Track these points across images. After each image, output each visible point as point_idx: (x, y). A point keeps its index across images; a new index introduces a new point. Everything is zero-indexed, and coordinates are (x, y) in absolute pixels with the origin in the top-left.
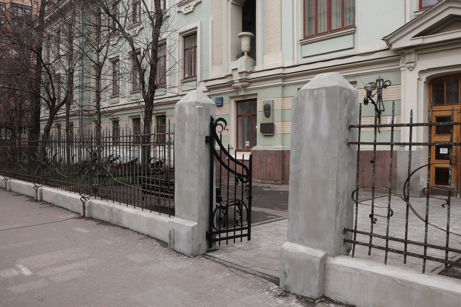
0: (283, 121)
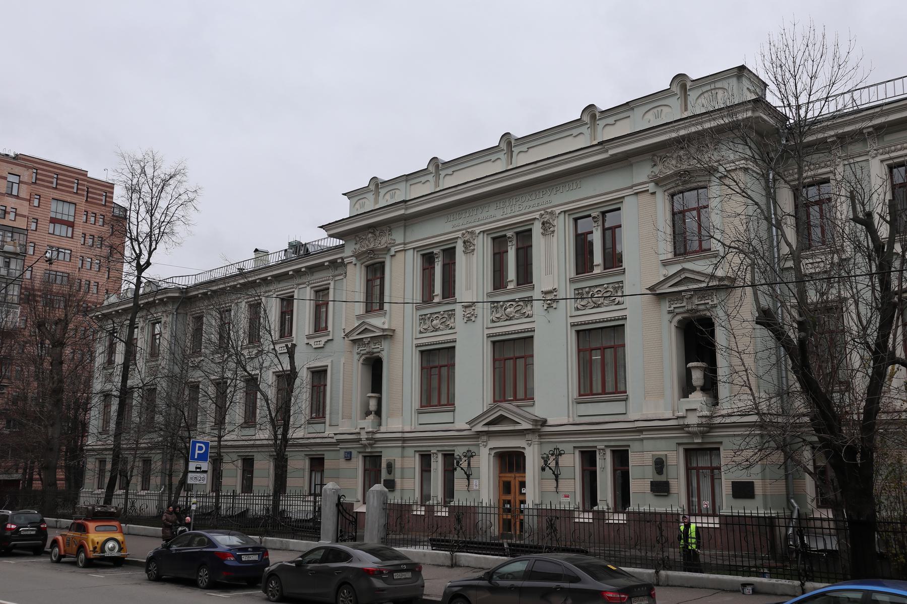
0: (402, 478)
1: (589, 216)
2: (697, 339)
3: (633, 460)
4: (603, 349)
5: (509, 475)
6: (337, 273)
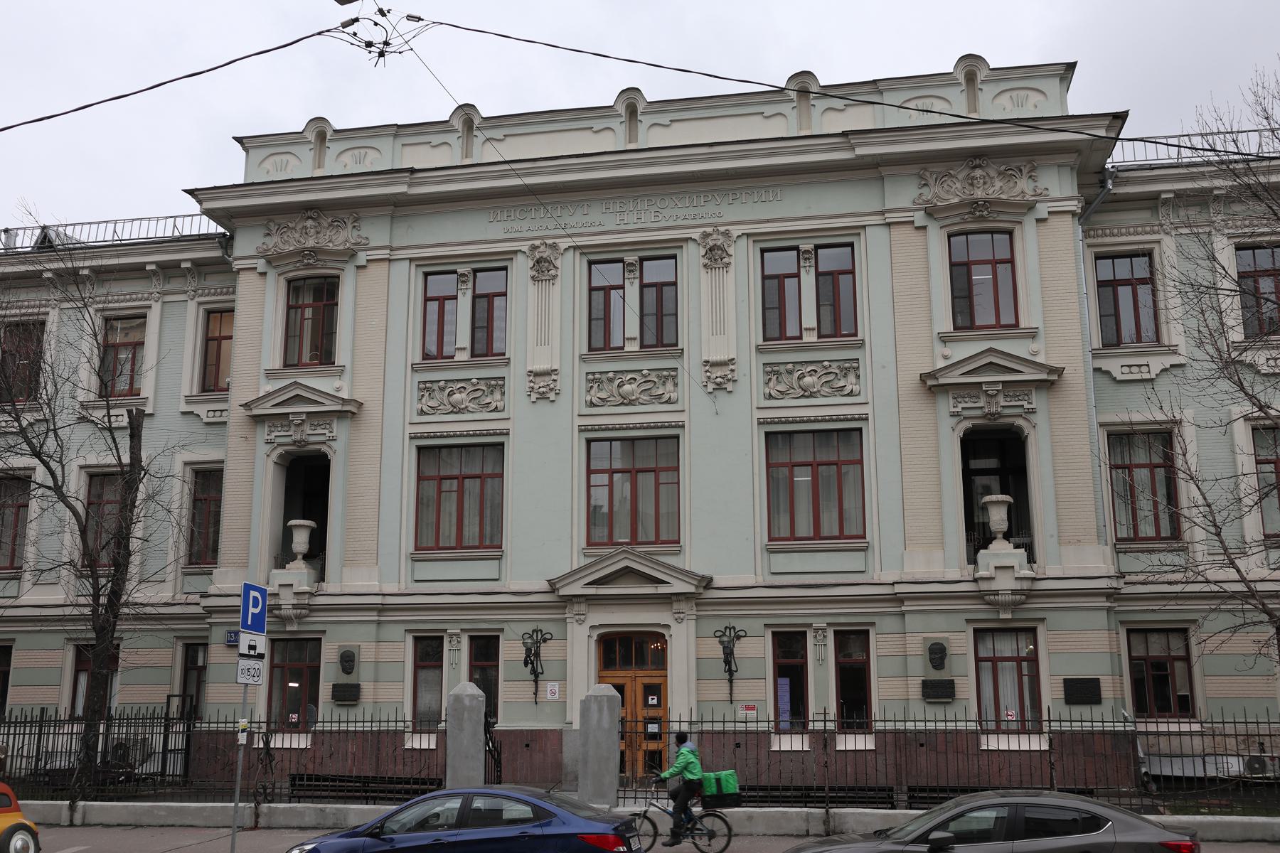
1: (455, 272)
2: (995, 458)
3: (880, 648)
4: (462, 478)
5: (622, 673)
6: (168, 287)
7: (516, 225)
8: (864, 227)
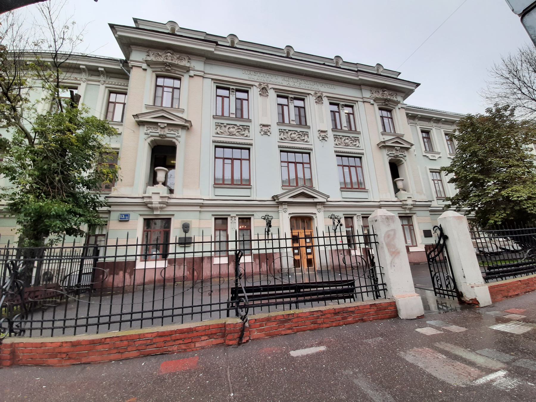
6: (90, 78)
7: (253, 77)
8: (357, 101)
